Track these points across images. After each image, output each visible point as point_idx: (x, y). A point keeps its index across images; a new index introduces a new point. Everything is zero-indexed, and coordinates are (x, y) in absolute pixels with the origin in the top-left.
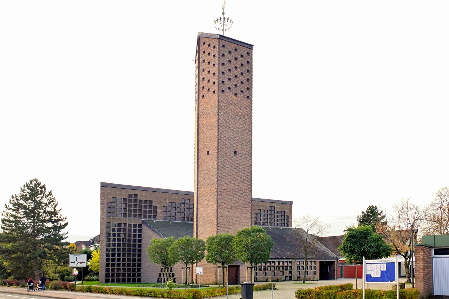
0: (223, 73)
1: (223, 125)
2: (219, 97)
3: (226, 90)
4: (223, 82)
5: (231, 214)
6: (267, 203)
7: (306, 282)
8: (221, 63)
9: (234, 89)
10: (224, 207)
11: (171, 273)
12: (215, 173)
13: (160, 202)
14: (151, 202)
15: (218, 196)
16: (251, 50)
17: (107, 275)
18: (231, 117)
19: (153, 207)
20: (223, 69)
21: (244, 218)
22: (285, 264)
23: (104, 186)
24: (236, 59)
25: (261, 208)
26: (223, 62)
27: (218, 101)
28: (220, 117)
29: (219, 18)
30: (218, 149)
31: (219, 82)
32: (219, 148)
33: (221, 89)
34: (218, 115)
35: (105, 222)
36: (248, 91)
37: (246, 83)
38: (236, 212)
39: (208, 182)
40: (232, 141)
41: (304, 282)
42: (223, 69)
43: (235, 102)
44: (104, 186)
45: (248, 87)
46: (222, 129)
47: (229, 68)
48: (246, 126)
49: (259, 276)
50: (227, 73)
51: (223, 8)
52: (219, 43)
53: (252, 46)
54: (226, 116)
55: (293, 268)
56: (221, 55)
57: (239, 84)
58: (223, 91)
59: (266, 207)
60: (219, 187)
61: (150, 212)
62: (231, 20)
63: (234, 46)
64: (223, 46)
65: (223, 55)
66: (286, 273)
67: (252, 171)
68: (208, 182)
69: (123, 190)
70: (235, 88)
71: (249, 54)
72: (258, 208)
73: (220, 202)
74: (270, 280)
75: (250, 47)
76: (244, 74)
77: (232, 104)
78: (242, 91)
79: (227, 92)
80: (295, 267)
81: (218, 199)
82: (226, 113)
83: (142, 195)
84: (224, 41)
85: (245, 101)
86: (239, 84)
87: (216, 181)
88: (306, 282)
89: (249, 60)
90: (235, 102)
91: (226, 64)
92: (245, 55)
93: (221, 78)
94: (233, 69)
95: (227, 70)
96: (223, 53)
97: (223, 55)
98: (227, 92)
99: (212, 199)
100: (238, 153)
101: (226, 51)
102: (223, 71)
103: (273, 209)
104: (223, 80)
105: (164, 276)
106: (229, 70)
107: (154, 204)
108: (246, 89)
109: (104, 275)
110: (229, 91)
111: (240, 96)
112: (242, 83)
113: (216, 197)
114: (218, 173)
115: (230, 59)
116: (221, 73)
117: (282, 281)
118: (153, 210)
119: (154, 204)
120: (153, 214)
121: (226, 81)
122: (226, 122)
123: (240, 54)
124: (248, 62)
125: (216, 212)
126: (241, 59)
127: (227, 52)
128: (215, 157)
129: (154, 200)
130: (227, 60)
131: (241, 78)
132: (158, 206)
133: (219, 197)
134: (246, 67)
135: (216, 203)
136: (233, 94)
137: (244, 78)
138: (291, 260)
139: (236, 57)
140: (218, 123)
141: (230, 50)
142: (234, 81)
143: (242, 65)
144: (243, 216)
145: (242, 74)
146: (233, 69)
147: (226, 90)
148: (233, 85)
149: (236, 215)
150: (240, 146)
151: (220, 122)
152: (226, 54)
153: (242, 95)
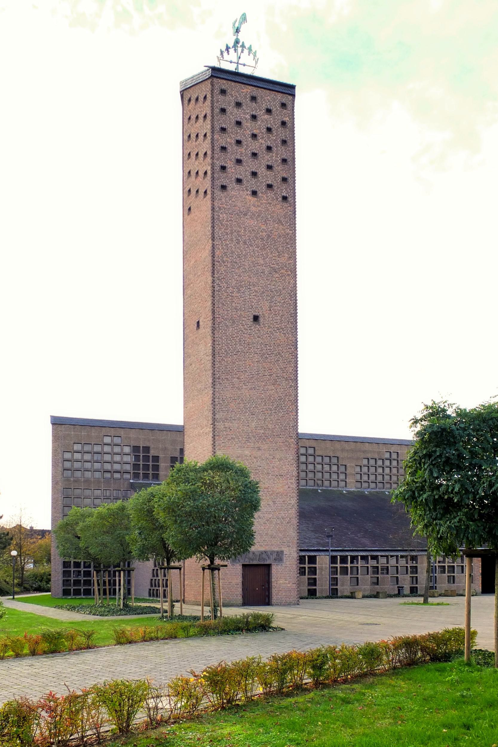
0: (223, 149)
1: (225, 259)
2: (213, 199)
3: (232, 185)
4: (223, 168)
5: (247, 452)
6: (381, 446)
7: (430, 600)
8: (217, 128)
9: (250, 183)
10: (229, 437)
11: (165, 578)
12: (209, 365)
13: (165, 449)
14: (147, 449)
15: (214, 414)
16: (290, 98)
17: (66, 582)
18: (245, 243)
19: (151, 458)
20: (222, 140)
21: (280, 460)
22: (393, 562)
23: (58, 423)
24: (254, 117)
25: (369, 456)
26: (224, 126)
27: (213, 209)
28: (216, 243)
29: (224, 49)
30: (213, 312)
31: (213, 168)
32: (216, 310)
33: (218, 183)
34: (213, 240)
35: (60, 487)
36: (284, 186)
37: (278, 168)
38: (259, 449)
39: (199, 386)
40: (247, 293)
41: (426, 602)
42: (222, 140)
43: (253, 209)
44: (58, 423)
45: (285, 175)
46: (222, 269)
47: (239, 138)
48: (282, 260)
49: (342, 585)
50: (232, 148)
51: (237, 31)
52: (212, 85)
53: (293, 87)
54: (232, 240)
55: (419, 570)
56: (217, 111)
57: (262, 171)
58: (224, 187)
59: (379, 453)
60: (217, 395)
61: (146, 467)
62: (250, 49)
63: (248, 90)
64: (223, 92)
65: (223, 111)
66: (404, 580)
67: (297, 357)
68: (199, 386)
69: (93, 430)
70: (254, 181)
71: (287, 106)
72: (362, 455)
73: (220, 426)
74: (360, 595)
75: (289, 90)
76: (274, 149)
77: (245, 215)
78: (270, 186)
79: (234, 190)
80: (423, 565)
81: (214, 420)
82: (232, 233)
83: (130, 438)
84: (225, 82)
85: (279, 206)
86: (262, 171)
87: (211, 381)
88: (430, 600)
89: (286, 119)
90: (253, 209)
91: (229, 130)
92: (276, 108)
93: (217, 160)
94: (247, 140)
95: (233, 142)
96: (223, 106)
97: (223, 111)
98: (234, 190)
99: (205, 422)
100: (261, 320)
101: (229, 103)
102: (224, 145)
103: (394, 456)
104: (223, 164)
105: (99, 590)
106: (239, 142)
107: (152, 453)
108: (279, 180)
109: (61, 582)
110: (237, 187)
111: (266, 196)
112: (269, 167)
113: (210, 415)
114: (214, 364)
115: (239, 119)
116: (217, 149)
117: (390, 596)
118: (151, 463)
119: (152, 453)
120: (151, 472)
121: (230, 165)
122: (232, 252)
123: (264, 106)
124: (284, 123)
125: (210, 447)
126: (266, 117)
127: (233, 104)
128: (209, 330)
129: (152, 446)
130: (233, 121)
131: (266, 158)
132: (161, 456)
133: (217, 416)
134: (280, 133)
135: (211, 429)
136: (249, 193)
137: (274, 158)
138: (414, 554)
139: (254, 113)
140: (213, 256)
141: (239, 100)
142: (250, 165)
143: (269, 130)
144: (278, 456)
145: (269, 148)
146: (247, 140)
147: (232, 185)
148: (248, 174)
149: (259, 453)
150: (267, 304)
151: (217, 253)
152: (230, 109)
153: (270, 194)
